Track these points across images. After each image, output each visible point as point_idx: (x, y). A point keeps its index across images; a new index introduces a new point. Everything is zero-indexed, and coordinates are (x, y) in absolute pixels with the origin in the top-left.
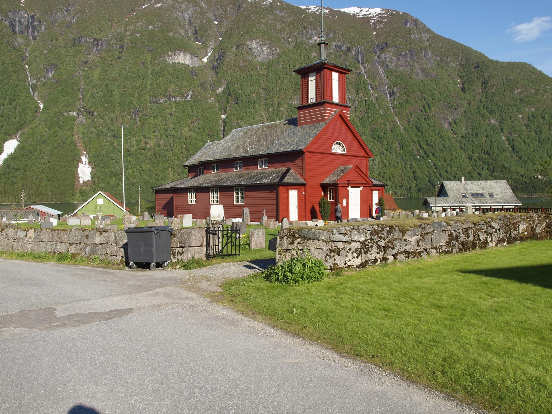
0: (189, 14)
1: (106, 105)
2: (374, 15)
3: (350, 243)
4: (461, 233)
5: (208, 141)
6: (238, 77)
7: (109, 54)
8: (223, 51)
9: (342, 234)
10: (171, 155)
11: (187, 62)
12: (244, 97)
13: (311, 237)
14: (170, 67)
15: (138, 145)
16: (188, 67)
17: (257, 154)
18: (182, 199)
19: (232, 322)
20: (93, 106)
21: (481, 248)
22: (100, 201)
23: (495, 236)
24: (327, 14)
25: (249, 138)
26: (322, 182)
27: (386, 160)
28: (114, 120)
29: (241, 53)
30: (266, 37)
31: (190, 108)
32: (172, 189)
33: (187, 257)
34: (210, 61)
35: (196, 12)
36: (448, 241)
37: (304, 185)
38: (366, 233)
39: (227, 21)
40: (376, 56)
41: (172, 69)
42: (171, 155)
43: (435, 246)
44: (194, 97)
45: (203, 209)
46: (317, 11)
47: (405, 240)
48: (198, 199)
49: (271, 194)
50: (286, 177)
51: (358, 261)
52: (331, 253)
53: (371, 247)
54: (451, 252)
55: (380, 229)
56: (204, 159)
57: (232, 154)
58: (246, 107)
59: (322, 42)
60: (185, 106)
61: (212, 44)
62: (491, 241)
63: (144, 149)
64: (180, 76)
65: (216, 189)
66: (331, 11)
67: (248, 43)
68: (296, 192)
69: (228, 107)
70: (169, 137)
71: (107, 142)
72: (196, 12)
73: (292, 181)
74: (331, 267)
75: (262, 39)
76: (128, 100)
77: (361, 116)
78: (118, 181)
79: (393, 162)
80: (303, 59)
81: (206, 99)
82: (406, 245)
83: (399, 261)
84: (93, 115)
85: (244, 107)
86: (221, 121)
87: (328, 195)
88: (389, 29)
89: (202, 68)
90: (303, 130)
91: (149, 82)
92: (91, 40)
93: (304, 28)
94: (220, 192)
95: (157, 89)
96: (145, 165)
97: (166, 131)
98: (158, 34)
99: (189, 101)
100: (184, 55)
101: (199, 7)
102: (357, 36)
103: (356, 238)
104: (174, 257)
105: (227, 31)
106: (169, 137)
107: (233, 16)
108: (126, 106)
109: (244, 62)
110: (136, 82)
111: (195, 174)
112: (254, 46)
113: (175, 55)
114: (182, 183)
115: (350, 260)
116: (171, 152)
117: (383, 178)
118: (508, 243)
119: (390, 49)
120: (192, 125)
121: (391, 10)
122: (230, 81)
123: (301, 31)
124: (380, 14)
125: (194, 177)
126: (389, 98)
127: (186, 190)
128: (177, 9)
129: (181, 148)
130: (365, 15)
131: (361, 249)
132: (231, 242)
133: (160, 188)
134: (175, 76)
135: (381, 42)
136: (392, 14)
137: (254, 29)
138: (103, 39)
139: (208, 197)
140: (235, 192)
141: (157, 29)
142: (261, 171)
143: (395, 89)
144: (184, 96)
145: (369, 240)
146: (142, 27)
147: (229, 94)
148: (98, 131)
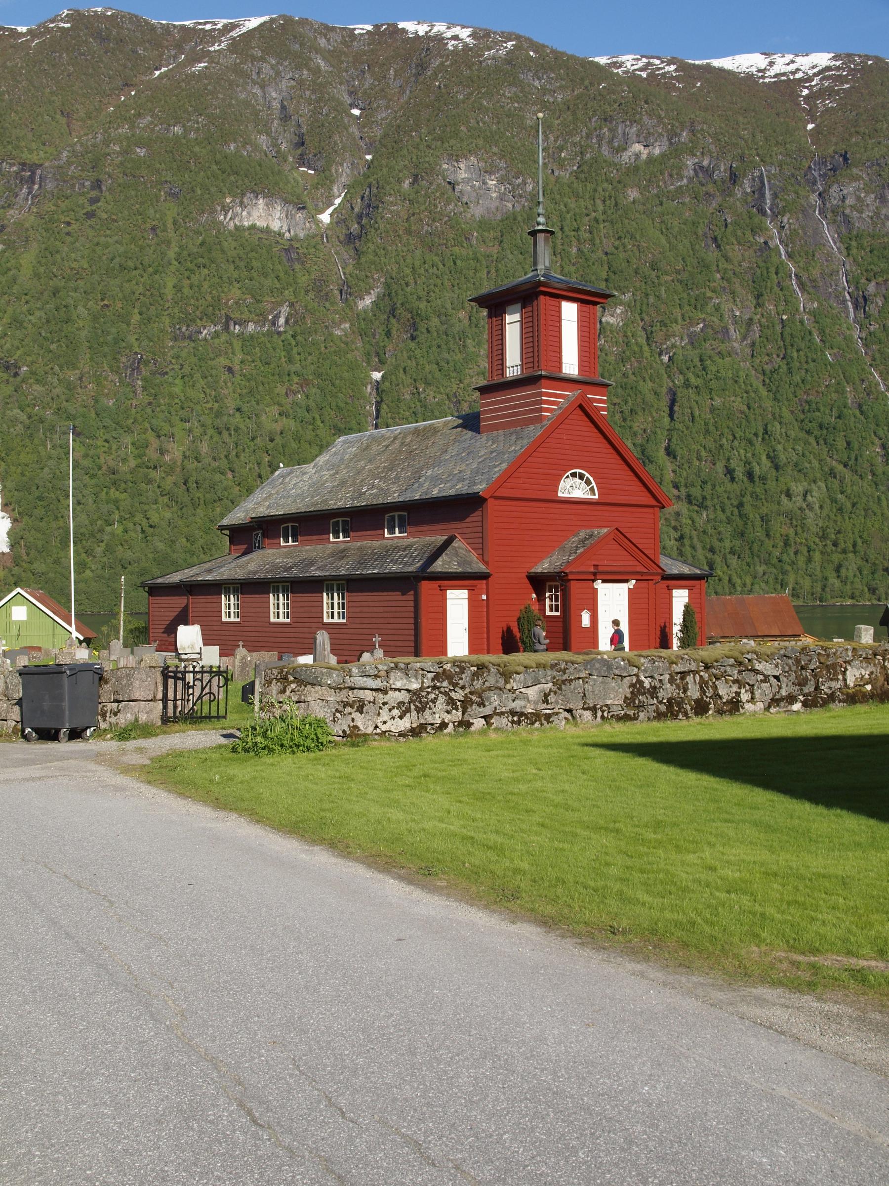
0: (281, 91)
1: (53, 347)
2: (811, 73)
3: (386, 693)
4: (666, 681)
5: (281, 465)
6: (417, 263)
7: (63, 205)
8: (374, 190)
9: (370, 676)
10: (231, 483)
11: (276, 226)
12: (435, 321)
13: (311, 679)
14: (230, 239)
15: (140, 456)
16: (279, 239)
17: (380, 501)
18: (209, 609)
19: (122, 789)
20: (18, 348)
21: (720, 712)
22: (19, 613)
23: (765, 691)
24: (672, 78)
25: (370, 461)
26: (533, 570)
27: (842, 493)
28: (75, 388)
29: (427, 196)
30: (495, 149)
31: (283, 353)
32: (185, 586)
33: (125, 719)
34: (339, 219)
35: (301, 83)
36: (629, 696)
37: (484, 577)
38: (423, 676)
39: (387, 108)
40: (814, 191)
41: (234, 244)
42: (231, 483)
43: (591, 705)
44: (296, 322)
45: (257, 634)
46: (641, 70)
47: (510, 690)
48: (295, 609)
49: (404, 597)
50: (440, 559)
51: (405, 724)
52: (344, 707)
53: (434, 701)
54: (635, 718)
55: (457, 670)
56: (263, 511)
57: (326, 500)
58: (439, 347)
59: (540, 227)
60: (269, 345)
61: (344, 173)
62: (752, 700)
63: (155, 467)
64: (255, 263)
65: (338, 585)
66: (683, 67)
67: (445, 166)
68: (464, 594)
69: (390, 347)
70: (225, 434)
71: (54, 447)
72: (301, 83)
73: (454, 568)
74: (344, 731)
75: (485, 156)
76: (114, 330)
77: (768, 368)
78: (84, 556)
79: (864, 499)
80: (601, 208)
81: (326, 327)
82: (514, 701)
83: (497, 729)
84: (16, 375)
85: (434, 348)
86: (369, 387)
87: (547, 600)
88: (854, 113)
89: (317, 238)
90: (490, 443)
91: (170, 282)
92: (15, 168)
93: (605, 120)
94: (292, 592)
95: (192, 302)
96: (157, 510)
97: (217, 417)
98: (197, 149)
99: (279, 333)
100: (267, 205)
101: (309, 69)
102: (759, 136)
103: (398, 685)
104: (105, 720)
105: (386, 135)
106: (225, 434)
107: (404, 92)
108: (106, 349)
109: (434, 220)
110: (134, 282)
111: (245, 546)
112: (463, 175)
113: (242, 204)
114: (209, 571)
115: (385, 723)
116: (230, 475)
117: (835, 544)
118: (805, 704)
119: (855, 171)
120: (290, 400)
121: (860, 56)
122: (394, 275)
123: (595, 129)
124: (828, 68)
125: (245, 554)
126: (852, 315)
127: (216, 588)
128: (248, 76)
129: (259, 464)
130: (784, 74)
131: (409, 703)
132: (210, 693)
133: (160, 580)
134: (242, 264)
135: (831, 151)
136: (865, 67)
137: (463, 128)
138: (47, 164)
139: (266, 605)
140: (325, 594)
141: (192, 135)
142: (390, 542)
143: (871, 288)
144: (266, 319)
145: (428, 687)
146: (153, 130)
147: (393, 312)
148: (30, 417)
